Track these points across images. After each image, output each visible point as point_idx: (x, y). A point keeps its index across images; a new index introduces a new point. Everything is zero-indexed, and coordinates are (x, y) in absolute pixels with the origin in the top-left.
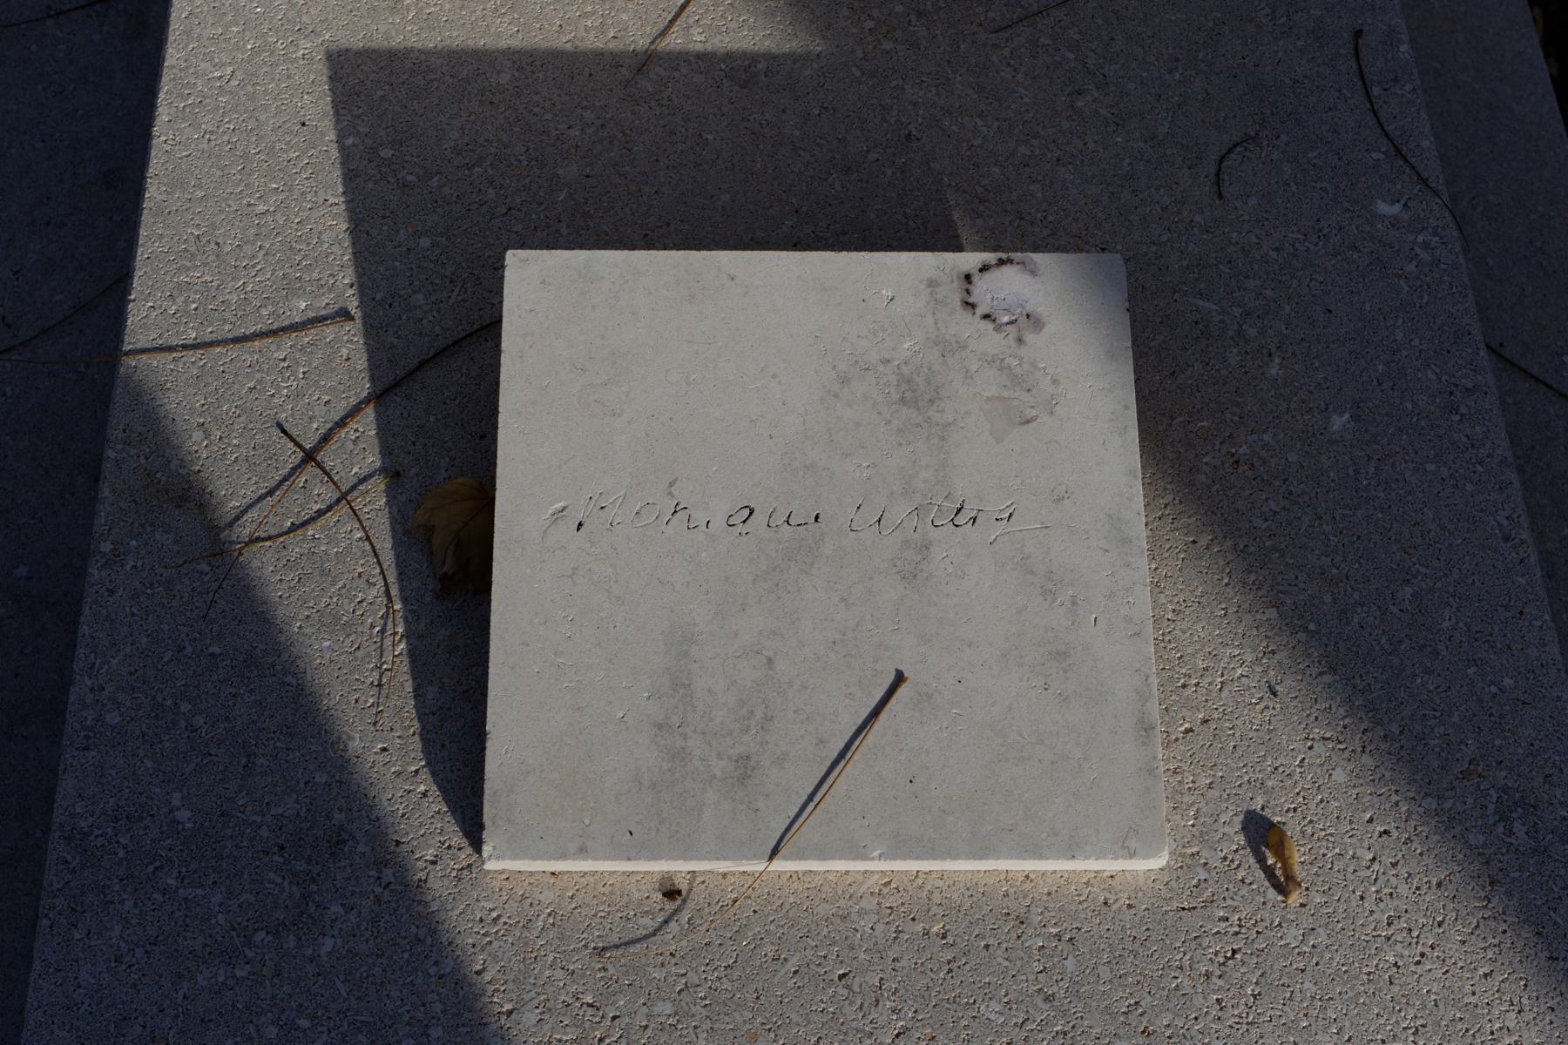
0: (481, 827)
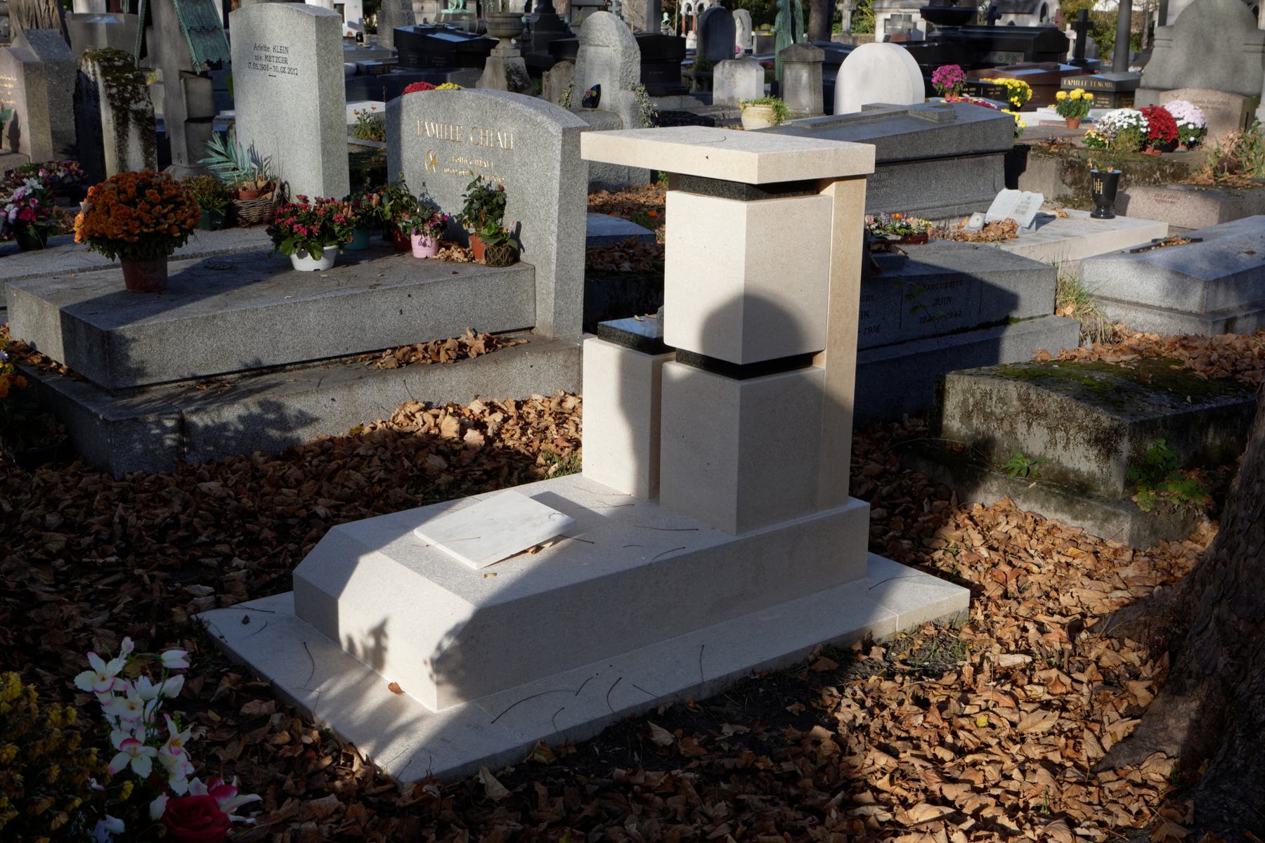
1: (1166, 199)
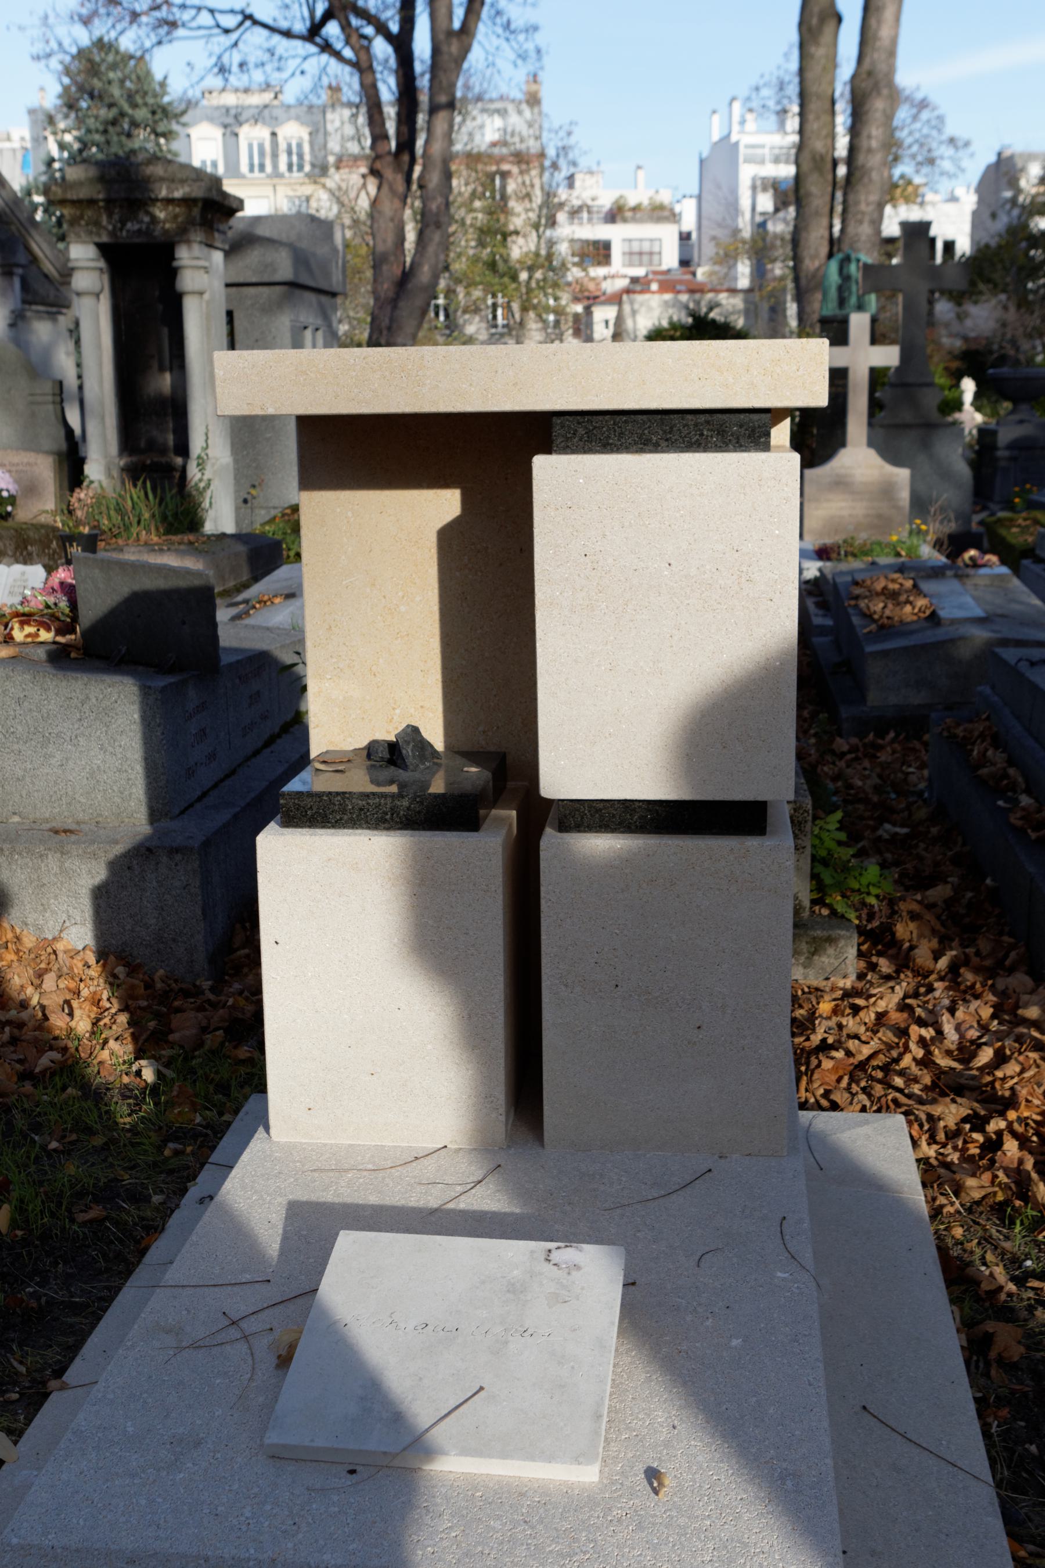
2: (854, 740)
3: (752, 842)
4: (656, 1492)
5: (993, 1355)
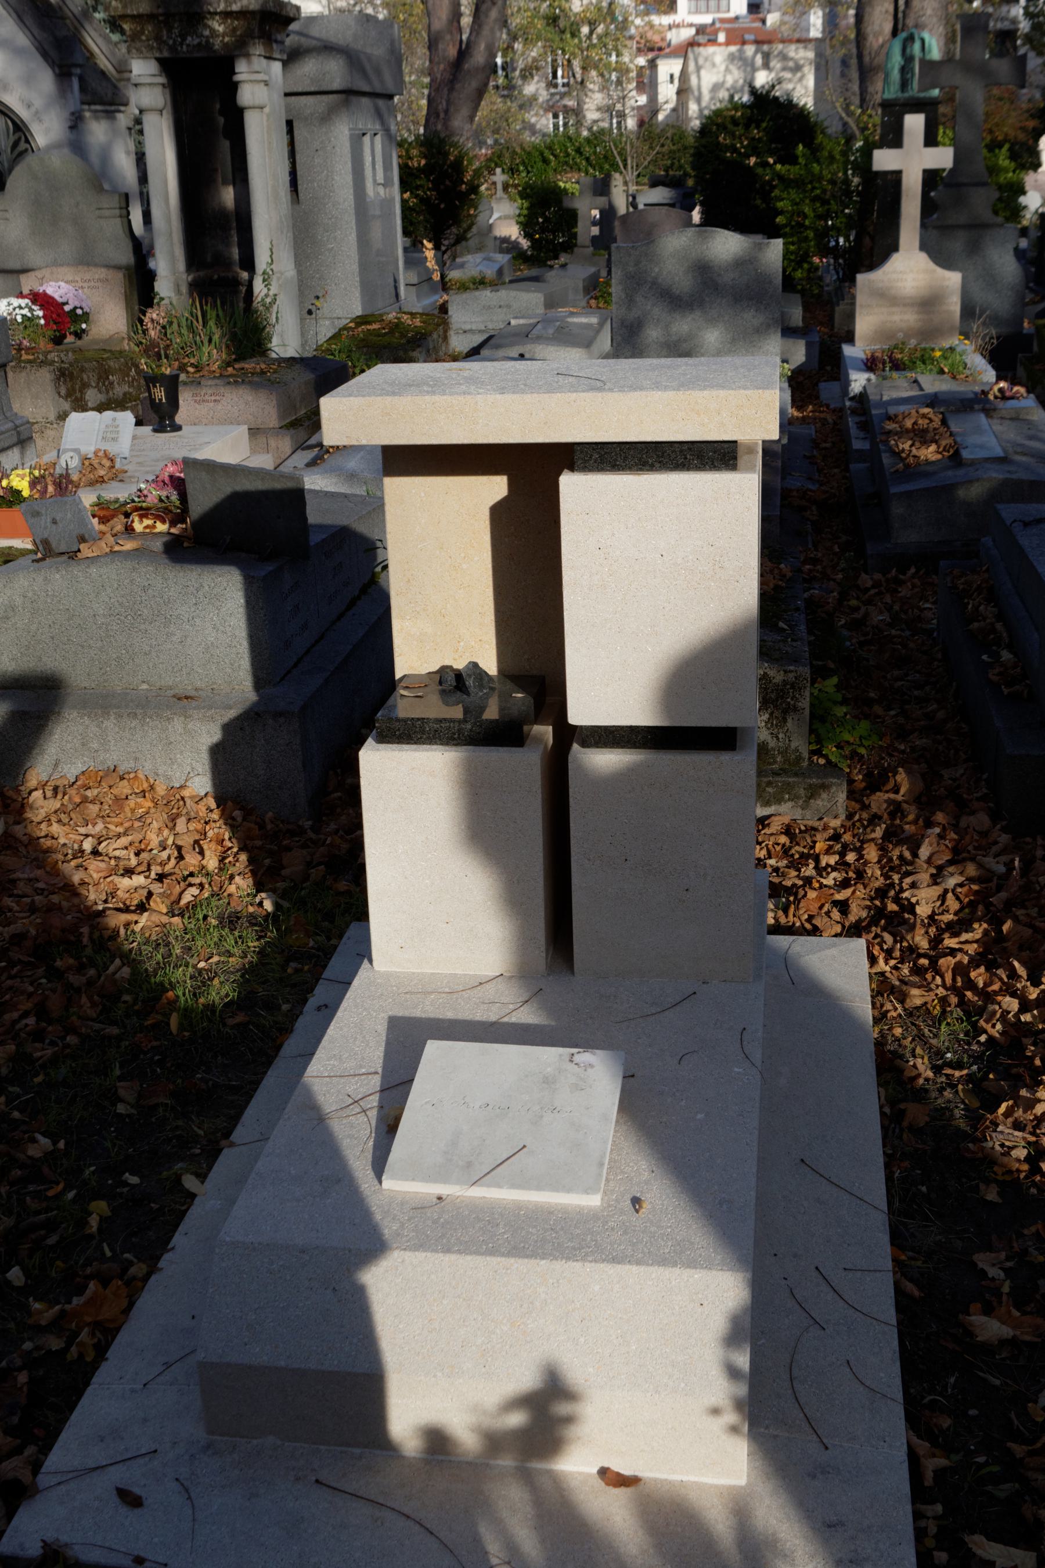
0: (383, 1172)
1: (207, 397)
2: (877, 576)
3: (725, 757)
4: (637, 1211)
5: (905, 1124)
